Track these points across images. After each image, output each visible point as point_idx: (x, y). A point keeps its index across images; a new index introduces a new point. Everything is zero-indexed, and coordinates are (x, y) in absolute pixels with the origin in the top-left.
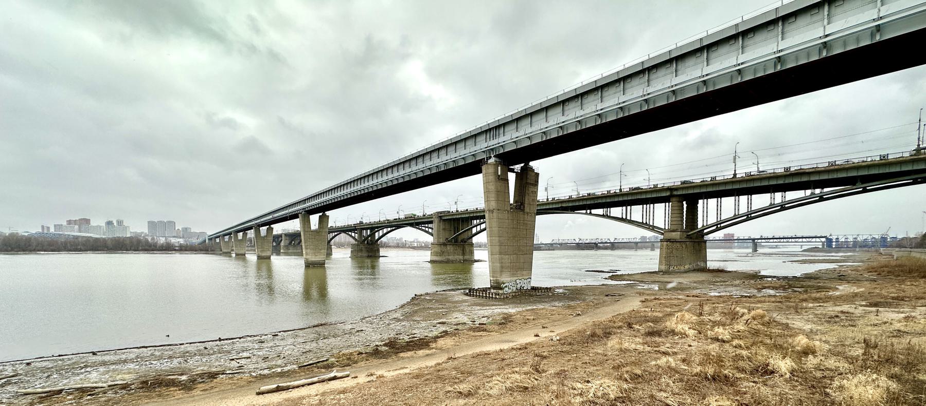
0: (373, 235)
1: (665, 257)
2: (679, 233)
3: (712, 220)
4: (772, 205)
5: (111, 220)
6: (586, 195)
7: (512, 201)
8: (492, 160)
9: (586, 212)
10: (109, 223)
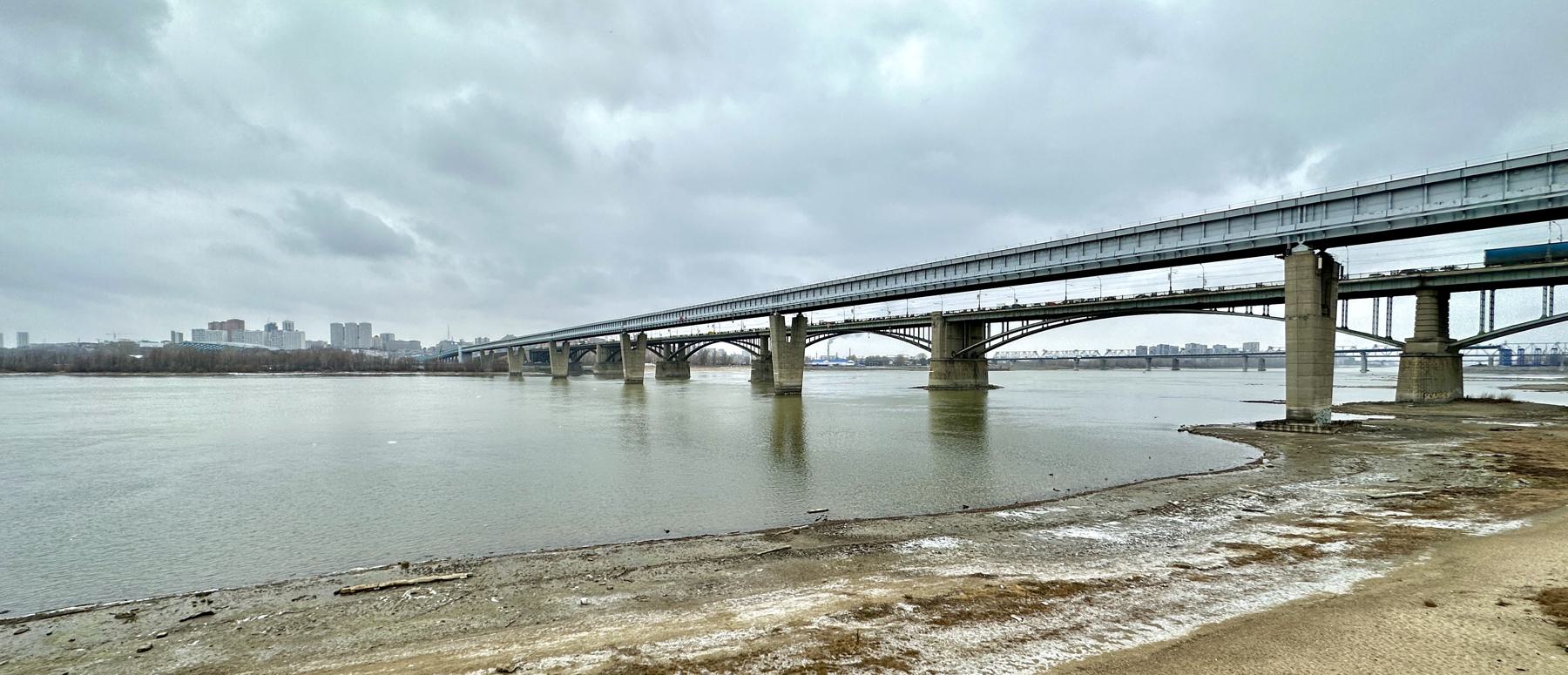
0: (491, 352)
1: (1417, 381)
2: (1437, 344)
5: (273, 322)
6: (1255, 286)
10: (271, 327)
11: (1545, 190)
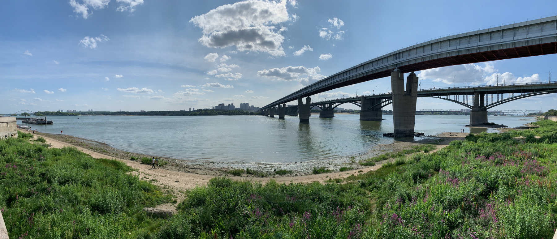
0: (330, 106)
3: (489, 103)
4: (509, 98)
7: (405, 90)
8: (396, 70)
9: (438, 97)
11: (539, 34)
